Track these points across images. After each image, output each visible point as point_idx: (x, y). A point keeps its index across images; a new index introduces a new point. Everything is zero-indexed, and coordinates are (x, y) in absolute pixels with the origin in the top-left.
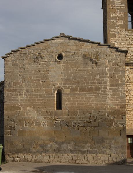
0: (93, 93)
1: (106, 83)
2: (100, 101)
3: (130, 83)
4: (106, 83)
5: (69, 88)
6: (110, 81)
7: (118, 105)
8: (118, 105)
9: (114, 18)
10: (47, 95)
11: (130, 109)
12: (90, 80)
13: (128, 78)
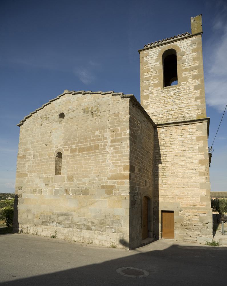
0: (93, 153)
1: (105, 138)
2: (88, 157)
3: (166, 147)
4: (107, 139)
5: (68, 150)
6: (112, 136)
7: (120, 166)
8: (120, 166)
9: (148, 79)
10: (50, 158)
11: (166, 179)
12: (89, 137)
13: (164, 141)
